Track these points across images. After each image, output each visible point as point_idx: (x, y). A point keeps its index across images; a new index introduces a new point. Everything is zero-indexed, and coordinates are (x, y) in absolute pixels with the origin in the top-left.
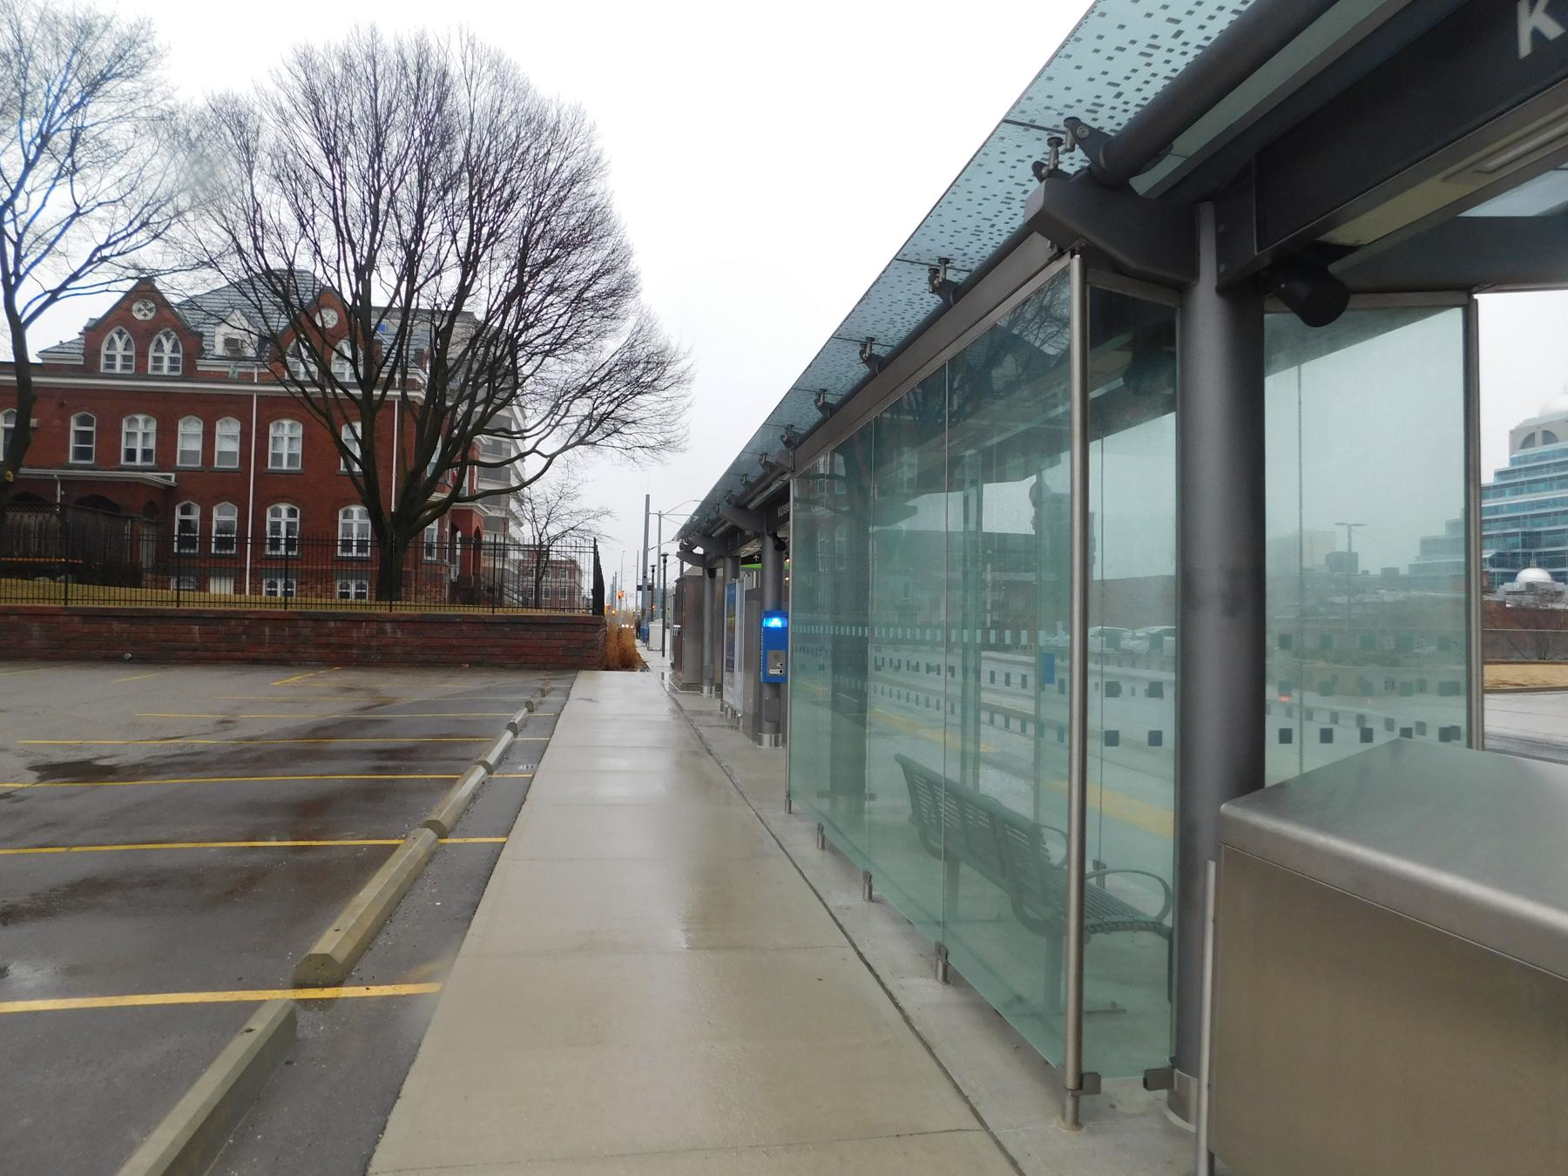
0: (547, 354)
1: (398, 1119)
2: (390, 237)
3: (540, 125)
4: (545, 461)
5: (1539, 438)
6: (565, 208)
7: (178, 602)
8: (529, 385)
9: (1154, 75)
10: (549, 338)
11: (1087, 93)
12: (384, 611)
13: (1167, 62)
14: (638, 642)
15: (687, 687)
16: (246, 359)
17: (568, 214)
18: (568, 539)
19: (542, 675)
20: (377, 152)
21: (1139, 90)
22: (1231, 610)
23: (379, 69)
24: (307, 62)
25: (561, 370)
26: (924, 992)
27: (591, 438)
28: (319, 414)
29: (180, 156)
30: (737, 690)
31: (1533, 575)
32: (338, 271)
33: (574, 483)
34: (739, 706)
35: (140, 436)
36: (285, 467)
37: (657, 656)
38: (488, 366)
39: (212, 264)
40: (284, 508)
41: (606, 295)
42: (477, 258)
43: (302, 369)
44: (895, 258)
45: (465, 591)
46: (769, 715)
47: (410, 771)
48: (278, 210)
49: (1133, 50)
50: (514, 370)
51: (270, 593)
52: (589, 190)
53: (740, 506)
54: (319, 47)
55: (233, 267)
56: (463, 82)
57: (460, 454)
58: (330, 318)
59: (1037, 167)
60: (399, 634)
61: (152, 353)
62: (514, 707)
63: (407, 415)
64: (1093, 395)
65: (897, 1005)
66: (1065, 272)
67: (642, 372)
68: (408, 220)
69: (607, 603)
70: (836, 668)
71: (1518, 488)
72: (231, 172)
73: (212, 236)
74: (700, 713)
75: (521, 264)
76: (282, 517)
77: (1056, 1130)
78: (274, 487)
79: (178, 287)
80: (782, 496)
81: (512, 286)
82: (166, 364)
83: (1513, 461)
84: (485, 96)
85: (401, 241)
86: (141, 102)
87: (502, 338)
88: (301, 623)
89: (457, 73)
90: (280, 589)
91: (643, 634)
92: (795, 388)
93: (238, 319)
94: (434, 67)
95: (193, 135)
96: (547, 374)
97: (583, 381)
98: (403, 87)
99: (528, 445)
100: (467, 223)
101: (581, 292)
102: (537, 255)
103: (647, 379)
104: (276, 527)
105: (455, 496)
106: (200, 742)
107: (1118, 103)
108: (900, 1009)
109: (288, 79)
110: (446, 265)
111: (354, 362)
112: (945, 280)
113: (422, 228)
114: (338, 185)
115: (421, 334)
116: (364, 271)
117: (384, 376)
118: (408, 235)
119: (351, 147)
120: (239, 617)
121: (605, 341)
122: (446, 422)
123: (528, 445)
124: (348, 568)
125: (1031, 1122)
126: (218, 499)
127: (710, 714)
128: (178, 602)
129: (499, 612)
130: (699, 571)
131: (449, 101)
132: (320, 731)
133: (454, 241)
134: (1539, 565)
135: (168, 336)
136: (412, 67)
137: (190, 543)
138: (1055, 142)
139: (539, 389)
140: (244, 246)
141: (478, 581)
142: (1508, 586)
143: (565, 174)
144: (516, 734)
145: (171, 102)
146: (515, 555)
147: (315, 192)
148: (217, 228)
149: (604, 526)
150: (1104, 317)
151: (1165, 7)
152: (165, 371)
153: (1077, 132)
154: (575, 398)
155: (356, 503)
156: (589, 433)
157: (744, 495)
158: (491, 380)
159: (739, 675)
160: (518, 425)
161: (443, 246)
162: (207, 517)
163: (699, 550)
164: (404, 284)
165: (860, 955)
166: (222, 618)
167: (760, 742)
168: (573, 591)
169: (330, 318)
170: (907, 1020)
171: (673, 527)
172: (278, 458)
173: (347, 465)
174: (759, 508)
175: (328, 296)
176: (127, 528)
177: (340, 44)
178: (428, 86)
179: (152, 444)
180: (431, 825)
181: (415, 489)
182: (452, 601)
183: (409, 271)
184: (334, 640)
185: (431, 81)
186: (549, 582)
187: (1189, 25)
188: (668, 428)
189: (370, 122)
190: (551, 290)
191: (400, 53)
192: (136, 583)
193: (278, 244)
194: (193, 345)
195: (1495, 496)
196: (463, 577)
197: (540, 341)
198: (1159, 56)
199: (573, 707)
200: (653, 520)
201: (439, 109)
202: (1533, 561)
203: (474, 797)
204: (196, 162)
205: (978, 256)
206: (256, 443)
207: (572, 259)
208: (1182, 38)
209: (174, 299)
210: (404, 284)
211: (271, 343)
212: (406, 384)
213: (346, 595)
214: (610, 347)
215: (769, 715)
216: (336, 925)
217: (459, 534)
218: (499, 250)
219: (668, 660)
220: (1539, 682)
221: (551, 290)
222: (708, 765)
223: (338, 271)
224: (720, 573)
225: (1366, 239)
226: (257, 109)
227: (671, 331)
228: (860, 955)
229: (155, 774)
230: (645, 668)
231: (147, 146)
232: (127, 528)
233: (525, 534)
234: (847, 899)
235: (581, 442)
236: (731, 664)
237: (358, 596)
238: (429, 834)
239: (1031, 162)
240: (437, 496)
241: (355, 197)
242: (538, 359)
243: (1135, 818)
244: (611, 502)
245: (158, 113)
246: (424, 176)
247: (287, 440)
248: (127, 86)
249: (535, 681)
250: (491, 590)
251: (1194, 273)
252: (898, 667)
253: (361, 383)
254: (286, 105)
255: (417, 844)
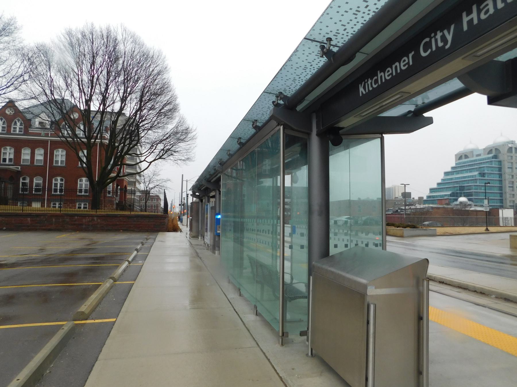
0: (149, 129)
1: (104, 350)
2: (97, 91)
3: (147, 56)
4: (148, 164)
5: (463, 157)
6: (156, 83)
7: (23, 210)
8: (143, 140)
9: (358, 22)
10: (149, 125)
11: (334, 28)
12: (94, 213)
13: (363, 17)
14: (179, 223)
15: (193, 237)
16: (46, 129)
17: (156, 85)
18: (156, 189)
19: (147, 234)
20: (93, 63)
21: (352, 28)
22: (320, 214)
23: (94, 37)
24: (69, 34)
25: (153, 135)
26: (250, 318)
27: (164, 157)
28: (72, 147)
29: (25, 62)
30: (208, 238)
31: (463, 199)
32: (79, 102)
33: (158, 171)
34: (209, 243)
35: (8, 154)
36: (59, 165)
37: (185, 228)
38: (128, 134)
39: (35, 98)
40: (59, 178)
41: (168, 111)
42: (126, 98)
43: (66, 132)
44: (305, 38)
45: (121, 206)
46: (216, 246)
47: (104, 263)
48: (59, 81)
49: (351, 12)
50: (138, 135)
51: (54, 207)
52: (164, 77)
53: (209, 181)
54: (74, 29)
55: (43, 99)
56: (122, 42)
57: (120, 161)
58: (76, 116)
59: (273, 102)
60: (99, 221)
61: (13, 126)
62: (137, 244)
63: (102, 148)
64: (286, 161)
65: (242, 321)
66: (280, 129)
67: (181, 135)
68: (103, 86)
69: (169, 209)
70: (235, 231)
71: (458, 172)
72: (43, 68)
73: (36, 89)
74: (198, 245)
75: (141, 101)
76: (58, 181)
77: (278, 347)
78: (55, 171)
79: (23, 105)
80: (219, 180)
81: (138, 108)
82: (18, 130)
83: (456, 164)
84: (129, 47)
85: (101, 93)
86: (11, 44)
87: (134, 124)
88: (66, 217)
89: (120, 39)
90: (57, 205)
91: (181, 220)
92: (221, 150)
93: (43, 115)
94: (112, 37)
95: (30, 55)
96: (148, 136)
97: (161, 138)
98: (102, 43)
99: (143, 159)
100: (123, 88)
101: (160, 110)
102: (146, 98)
103: (182, 138)
104: (56, 185)
105: (118, 176)
106: (34, 256)
107: (312, 67)
108: (243, 322)
109: (63, 39)
110: (116, 100)
111: (84, 132)
112: (278, 103)
113: (108, 89)
114: (80, 74)
115: (107, 123)
116: (88, 102)
117: (95, 135)
118: (103, 90)
119: (84, 62)
120: (44, 215)
121: (168, 126)
122: (116, 151)
123: (143, 159)
124: (81, 199)
125: (270, 344)
126: (36, 175)
127: (201, 245)
128: (23, 210)
129: (133, 213)
130: (198, 200)
131: (117, 48)
132: (73, 252)
133: (119, 93)
134: (464, 196)
135: (19, 120)
136: (105, 37)
137: (26, 190)
138: (277, 97)
139: (147, 141)
140: (48, 93)
141: (125, 203)
142: (455, 203)
143: (155, 72)
144: (138, 252)
145: (22, 44)
146: (138, 194)
147: (72, 76)
148: (37, 87)
149: (168, 184)
150: (290, 142)
151: (340, 21)
152: (17, 132)
153: (280, 95)
154: (158, 143)
155: (84, 177)
156: (163, 155)
157: (210, 178)
158: (130, 138)
159: (209, 233)
160: (140, 152)
161: (115, 95)
162: (31, 181)
163: (197, 194)
164: (102, 106)
165: (235, 310)
166: (38, 215)
167: (214, 253)
168: (158, 206)
169: (76, 116)
170: (244, 324)
171: (190, 186)
172: (57, 162)
173: (81, 164)
174: (214, 182)
175: (74, 108)
176: (3, 186)
177: (81, 28)
178: (111, 43)
179: (12, 156)
180: (112, 278)
181: (104, 174)
182: (117, 209)
183: (104, 101)
184: (77, 223)
185: (111, 41)
186: (149, 203)
187: (348, 27)
188: (188, 154)
189: (91, 53)
190: (151, 109)
191: (101, 32)
192: (6, 204)
193: (59, 93)
194: (27, 124)
195: (451, 175)
196: (120, 202)
197: (146, 125)
198: (360, 15)
199: (157, 243)
200: (185, 183)
201: (114, 50)
202: (463, 195)
203: (124, 270)
204: (31, 64)
205: (295, 89)
206: (49, 156)
207: (158, 99)
208: (346, 31)
209: (21, 108)
210: (102, 106)
211: (55, 124)
212: (102, 138)
213: (80, 208)
214: (170, 127)
215: (216, 246)
216: (85, 304)
217: (119, 187)
218: (133, 96)
219: (188, 229)
220: (457, 233)
221: (151, 109)
222: (197, 261)
223: (79, 102)
224: (204, 200)
225: (345, 126)
226: (53, 49)
227: (190, 123)
228: (235, 310)
229: (21, 266)
230: (181, 231)
231: (14, 59)
232: (3, 186)
233: (142, 187)
234: (233, 295)
235: (160, 158)
236: (207, 229)
237: (85, 208)
238: (111, 281)
239: (272, 101)
240: (113, 175)
241: (86, 78)
242: (146, 131)
243: (294, 268)
244: (170, 177)
245: (18, 48)
246: (108, 73)
247: (60, 156)
248: (6, 39)
249: (144, 235)
250: (130, 206)
251: (311, 130)
252: (263, 230)
253: (86, 138)
254: (62, 47)
255: (107, 284)
